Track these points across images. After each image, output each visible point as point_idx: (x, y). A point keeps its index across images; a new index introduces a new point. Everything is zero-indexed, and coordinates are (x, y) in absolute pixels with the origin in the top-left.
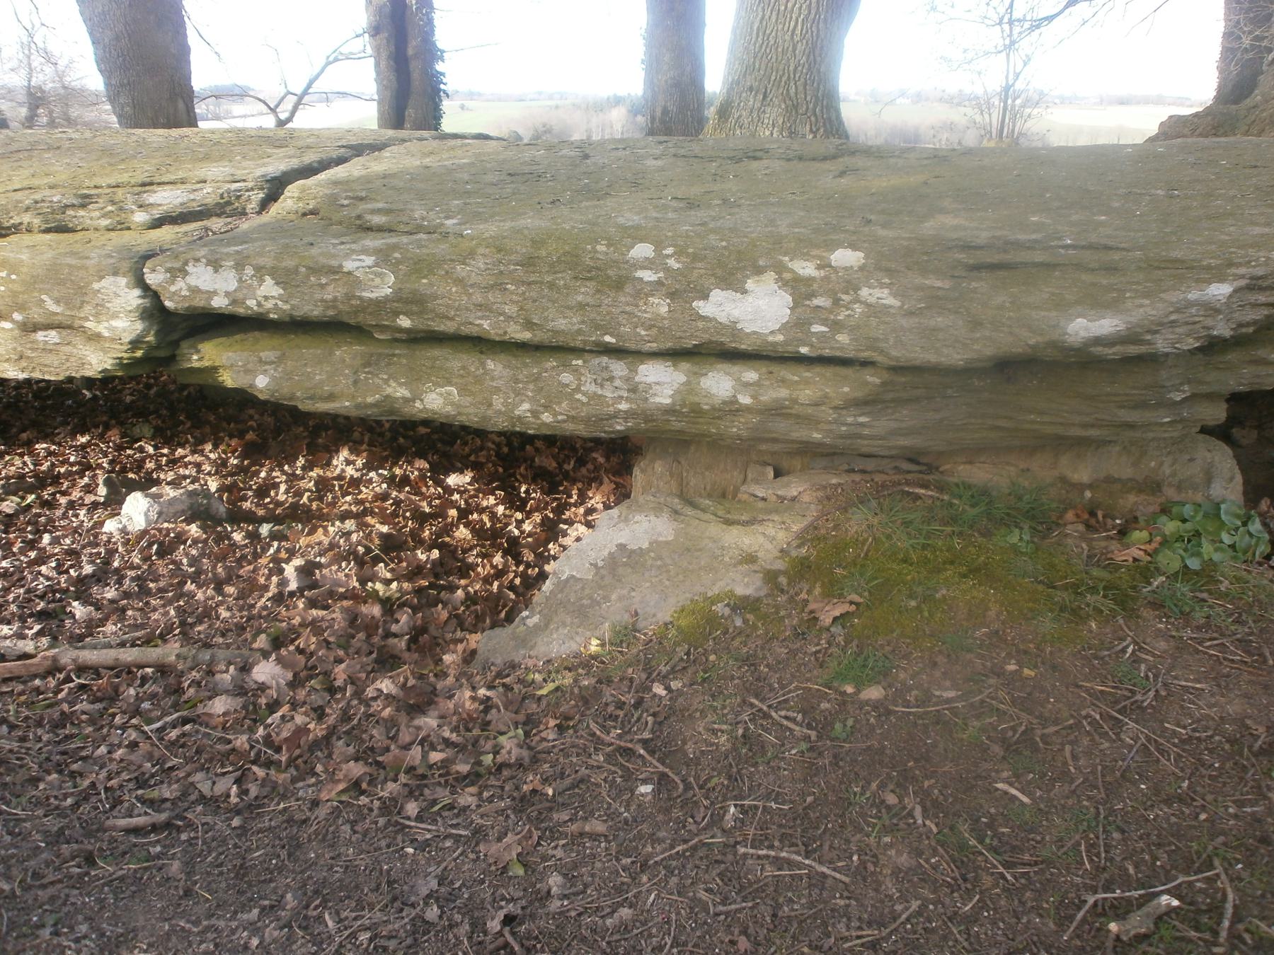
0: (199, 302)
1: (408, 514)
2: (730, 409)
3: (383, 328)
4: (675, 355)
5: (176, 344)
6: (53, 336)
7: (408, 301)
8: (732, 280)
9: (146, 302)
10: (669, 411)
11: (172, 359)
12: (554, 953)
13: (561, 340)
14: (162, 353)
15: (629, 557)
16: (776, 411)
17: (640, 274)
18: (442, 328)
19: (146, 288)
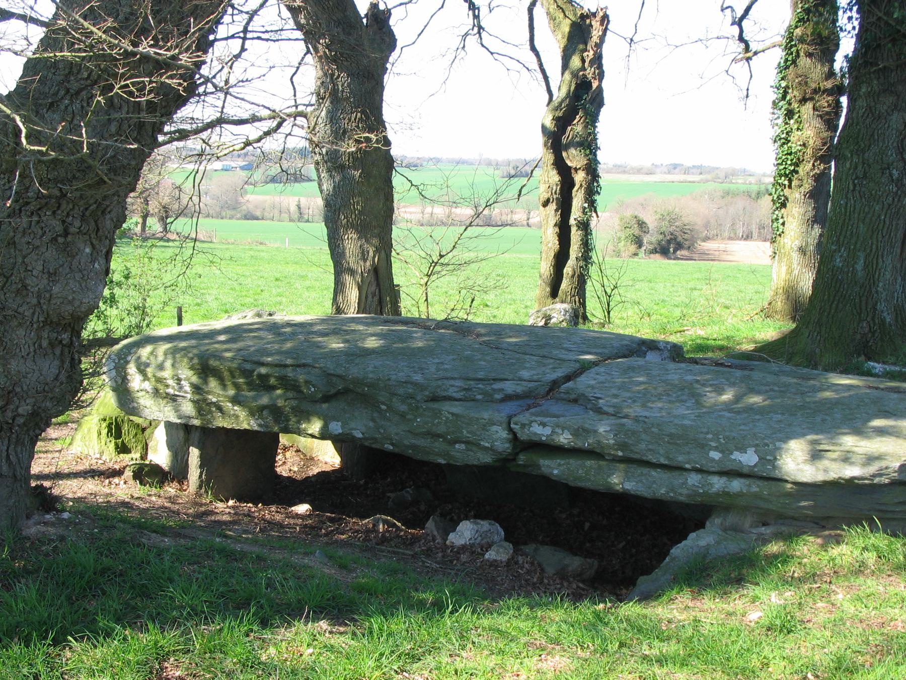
0: (534, 438)
1: (634, 551)
2: (740, 495)
3: (610, 454)
4: (721, 473)
5: (517, 454)
6: (463, 446)
7: (623, 446)
8: (743, 450)
9: (510, 436)
10: (717, 494)
11: (514, 460)
12: (112, 676)
13: (679, 465)
14: (510, 457)
15: (26, 426)
16: (756, 496)
17: (711, 443)
18: (634, 457)
19: (511, 430)
